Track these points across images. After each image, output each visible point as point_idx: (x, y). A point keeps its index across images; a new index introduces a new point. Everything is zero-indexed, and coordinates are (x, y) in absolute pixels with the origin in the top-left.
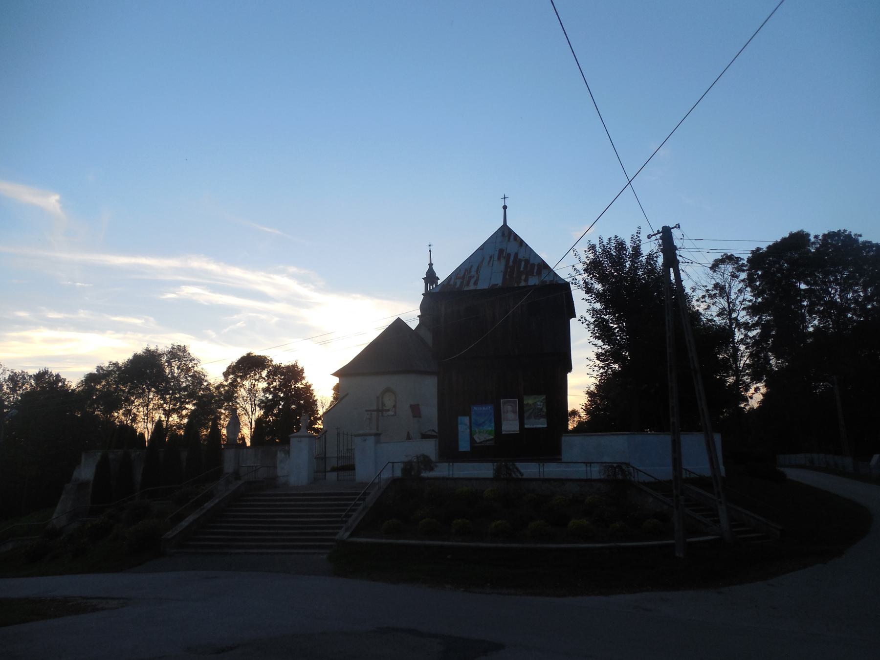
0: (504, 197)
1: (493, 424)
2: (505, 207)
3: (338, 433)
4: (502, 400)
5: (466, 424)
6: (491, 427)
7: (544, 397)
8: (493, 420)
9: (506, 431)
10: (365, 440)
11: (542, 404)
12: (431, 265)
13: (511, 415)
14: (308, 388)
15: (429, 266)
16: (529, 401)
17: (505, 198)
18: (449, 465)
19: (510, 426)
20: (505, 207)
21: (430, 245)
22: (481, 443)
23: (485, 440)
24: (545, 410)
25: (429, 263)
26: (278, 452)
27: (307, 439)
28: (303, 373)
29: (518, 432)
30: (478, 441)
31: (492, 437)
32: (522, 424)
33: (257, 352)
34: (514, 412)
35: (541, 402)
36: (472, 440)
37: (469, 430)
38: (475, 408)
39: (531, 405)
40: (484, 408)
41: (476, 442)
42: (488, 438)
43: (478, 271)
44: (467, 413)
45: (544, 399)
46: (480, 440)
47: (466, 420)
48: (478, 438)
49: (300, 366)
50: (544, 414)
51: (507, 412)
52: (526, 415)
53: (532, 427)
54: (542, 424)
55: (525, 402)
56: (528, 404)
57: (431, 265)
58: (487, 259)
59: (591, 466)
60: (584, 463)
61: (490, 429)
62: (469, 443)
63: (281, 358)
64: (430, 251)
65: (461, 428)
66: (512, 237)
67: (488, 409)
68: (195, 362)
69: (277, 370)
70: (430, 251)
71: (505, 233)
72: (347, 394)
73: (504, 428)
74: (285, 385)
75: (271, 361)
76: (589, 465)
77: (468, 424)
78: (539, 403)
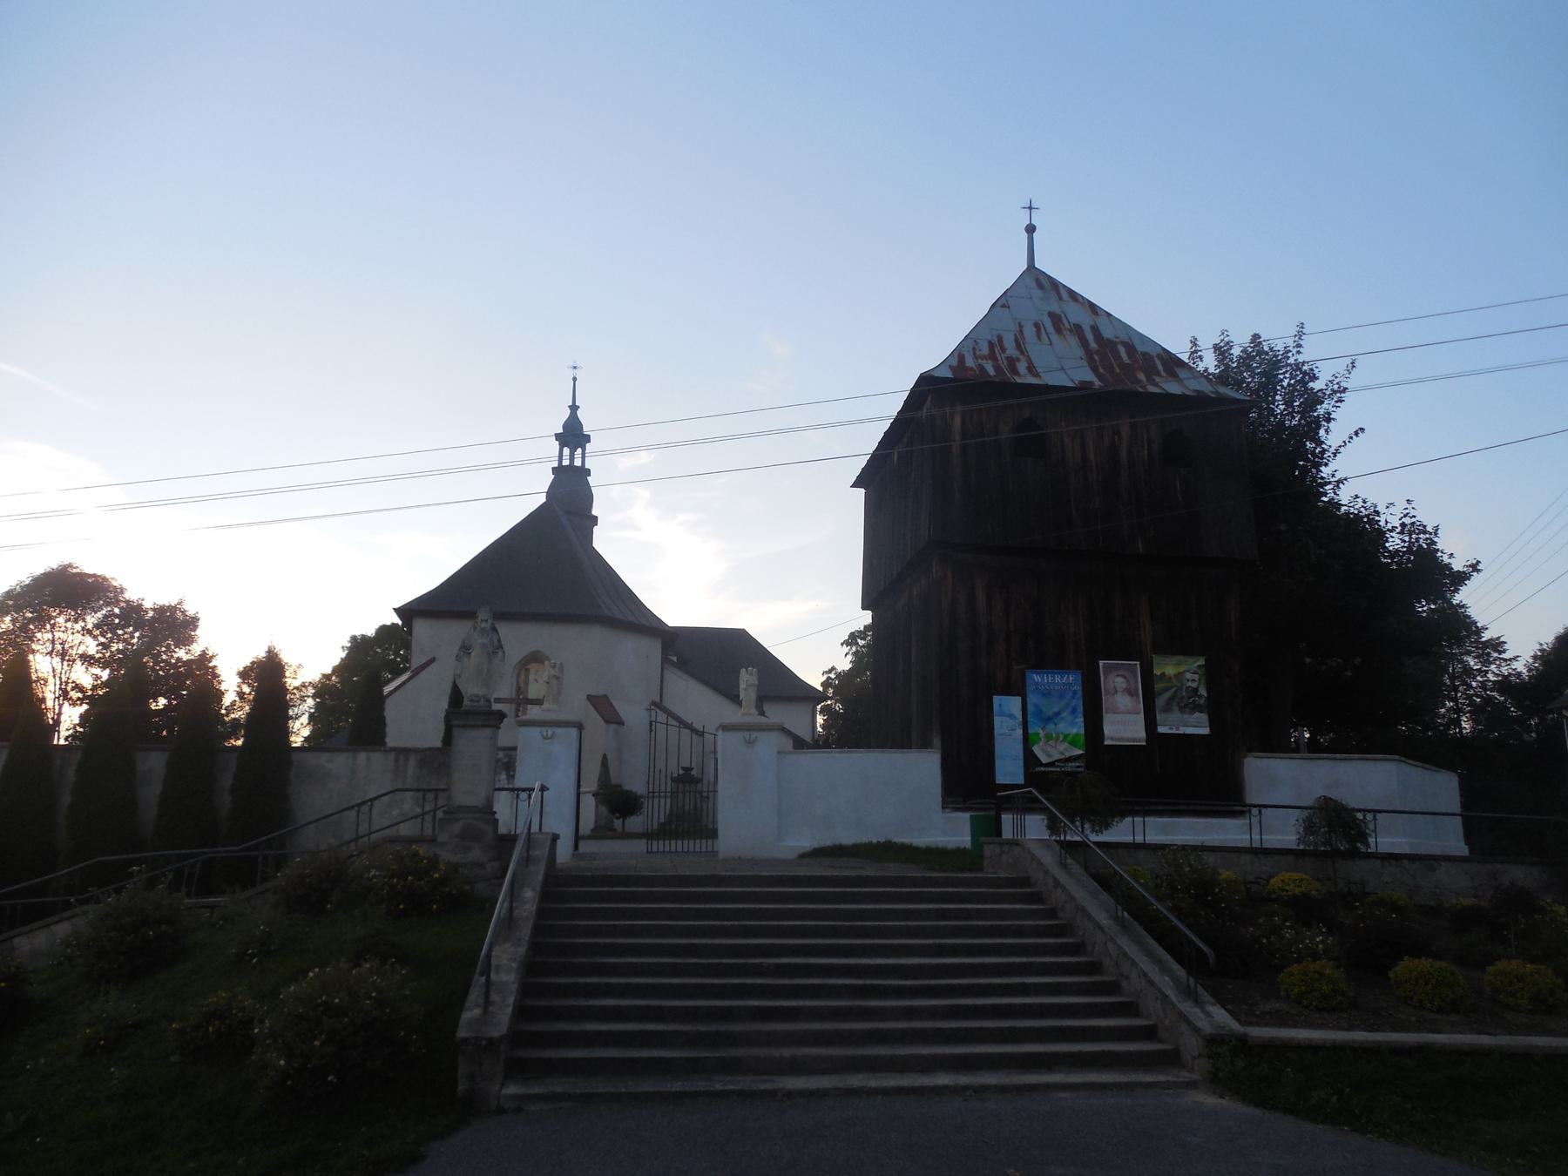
0: (1033, 211)
1: (1080, 719)
2: (1031, 229)
3: (651, 722)
4: (1101, 663)
5: (1012, 716)
6: (1077, 728)
7: (1201, 662)
8: (1081, 708)
9: (1112, 739)
10: (750, 743)
12: (574, 408)
13: (1123, 701)
14: (204, 658)
15: (569, 411)
16: (1166, 667)
20: (1031, 229)
22: (1052, 764)
24: (1203, 692)
25: (571, 404)
26: (1483, 639)
28: (195, 627)
29: (1144, 744)
30: (1045, 760)
31: (1081, 752)
33: (88, 564)
34: (1130, 692)
35: (1195, 673)
36: (1030, 758)
37: (1020, 732)
38: (1037, 678)
39: (1170, 678)
40: (1057, 679)
41: (1039, 762)
42: (1068, 755)
43: (1019, 346)
44: (1015, 687)
45: (1199, 666)
46: (1049, 756)
47: (1012, 704)
50: (1202, 702)
51: (1116, 692)
52: (1160, 702)
53: (1174, 731)
54: (1197, 725)
55: (1157, 672)
57: (574, 408)
58: (1029, 332)
61: (1074, 731)
62: (1021, 763)
64: (575, 379)
65: (1000, 725)
66: (1065, 295)
67: (1070, 680)
69: (133, 613)
70: (575, 379)
71: (1036, 280)
72: (432, 660)
74: (148, 647)
75: (122, 590)
77: (1019, 715)
78: (1188, 676)
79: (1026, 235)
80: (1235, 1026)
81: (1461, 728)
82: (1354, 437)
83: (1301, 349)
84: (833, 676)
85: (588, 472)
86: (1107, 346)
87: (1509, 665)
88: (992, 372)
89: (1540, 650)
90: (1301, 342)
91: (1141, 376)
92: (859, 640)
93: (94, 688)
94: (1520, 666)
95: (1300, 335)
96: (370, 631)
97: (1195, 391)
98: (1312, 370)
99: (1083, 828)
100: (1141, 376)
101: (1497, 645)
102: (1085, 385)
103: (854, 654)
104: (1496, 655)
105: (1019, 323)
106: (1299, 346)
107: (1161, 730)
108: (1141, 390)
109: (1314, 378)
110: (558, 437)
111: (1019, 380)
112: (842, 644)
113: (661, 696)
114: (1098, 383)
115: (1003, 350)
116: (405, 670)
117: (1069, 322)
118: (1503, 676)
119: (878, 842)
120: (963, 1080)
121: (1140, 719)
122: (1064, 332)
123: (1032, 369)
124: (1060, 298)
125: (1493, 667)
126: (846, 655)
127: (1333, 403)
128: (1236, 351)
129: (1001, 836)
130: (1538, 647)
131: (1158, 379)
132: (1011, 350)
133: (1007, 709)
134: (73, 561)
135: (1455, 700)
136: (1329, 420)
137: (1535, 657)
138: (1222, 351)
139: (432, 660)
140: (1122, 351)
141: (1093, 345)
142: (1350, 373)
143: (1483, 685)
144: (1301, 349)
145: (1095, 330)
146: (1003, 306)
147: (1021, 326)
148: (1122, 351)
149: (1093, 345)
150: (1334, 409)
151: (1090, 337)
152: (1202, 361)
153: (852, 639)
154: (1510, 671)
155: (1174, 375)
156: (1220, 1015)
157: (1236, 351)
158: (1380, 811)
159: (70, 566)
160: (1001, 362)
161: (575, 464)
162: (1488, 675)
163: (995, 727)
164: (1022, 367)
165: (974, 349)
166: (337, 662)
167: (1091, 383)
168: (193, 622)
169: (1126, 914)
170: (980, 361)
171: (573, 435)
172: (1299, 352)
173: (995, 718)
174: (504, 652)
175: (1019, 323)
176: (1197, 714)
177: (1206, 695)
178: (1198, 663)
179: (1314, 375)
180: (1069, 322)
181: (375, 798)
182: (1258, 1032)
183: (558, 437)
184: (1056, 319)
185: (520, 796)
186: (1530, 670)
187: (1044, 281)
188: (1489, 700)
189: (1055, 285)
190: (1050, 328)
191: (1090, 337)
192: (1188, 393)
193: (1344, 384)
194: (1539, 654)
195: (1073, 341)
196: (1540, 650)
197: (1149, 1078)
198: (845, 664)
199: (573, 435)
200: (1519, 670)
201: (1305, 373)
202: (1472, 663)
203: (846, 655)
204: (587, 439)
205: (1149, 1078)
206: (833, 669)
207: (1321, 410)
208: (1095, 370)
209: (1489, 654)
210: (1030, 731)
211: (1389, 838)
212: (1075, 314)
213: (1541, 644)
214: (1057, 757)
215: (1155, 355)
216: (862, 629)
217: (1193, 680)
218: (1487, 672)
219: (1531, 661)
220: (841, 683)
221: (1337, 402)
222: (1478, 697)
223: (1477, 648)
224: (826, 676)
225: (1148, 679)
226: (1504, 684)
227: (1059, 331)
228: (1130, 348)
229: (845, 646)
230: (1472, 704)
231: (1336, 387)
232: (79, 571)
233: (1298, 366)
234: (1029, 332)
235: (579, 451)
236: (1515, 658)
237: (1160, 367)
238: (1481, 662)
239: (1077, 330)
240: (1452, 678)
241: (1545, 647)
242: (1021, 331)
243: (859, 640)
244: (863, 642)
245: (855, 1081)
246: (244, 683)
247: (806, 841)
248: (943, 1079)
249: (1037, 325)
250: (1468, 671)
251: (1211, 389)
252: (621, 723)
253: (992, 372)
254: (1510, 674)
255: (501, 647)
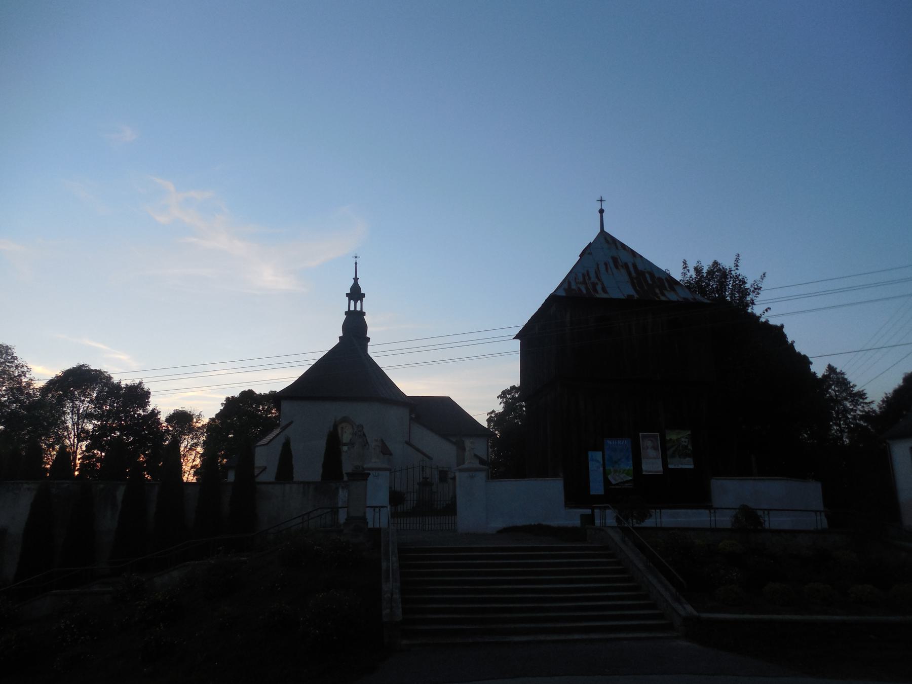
2: (601, 211)
4: (640, 434)
5: (598, 461)
6: (629, 466)
7: (689, 432)
9: (646, 471)
11: (687, 440)
12: (356, 279)
13: (651, 453)
16: (672, 436)
17: (601, 201)
18: (710, 512)
19: (652, 465)
21: (356, 257)
22: (617, 484)
23: (622, 481)
24: (690, 447)
26: (340, 490)
27: (388, 473)
29: (662, 473)
30: (614, 482)
31: (630, 478)
32: (665, 464)
34: (655, 448)
35: (687, 438)
36: (607, 482)
40: (619, 442)
41: (610, 483)
42: (625, 480)
43: (597, 277)
44: (599, 447)
47: (598, 455)
48: (614, 479)
49: (146, 387)
51: (648, 448)
53: (676, 467)
54: (687, 464)
55: (668, 438)
56: (671, 439)
57: (356, 279)
58: (602, 268)
59: (769, 513)
60: (812, 511)
61: (628, 468)
63: (123, 376)
64: (356, 263)
65: (592, 466)
66: (619, 246)
68: (25, 369)
70: (356, 263)
71: (605, 239)
73: (644, 467)
76: (818, 513)
77: (601, 460)
79: (599, 214)
80: (695, 613)
81: (843, 442)
82: (766, 312)
83: (738, 268)
84: (493, 415)
85: (364, 314)
86: (640, 274)
87: (869, 406)
88: (585, 292)
89: (885, 397)
90: (738, 264)
91: (657, 291)
92: (508, 395)
93: (94, 430)
94: (875, 407)
95: (737, 260)
96: (237, 395)
97: (684, 298)
98: (743, 279)
99: (632, 521)
100: (657, 291)
101: (861, 395)
102: (630, 298)
103: (504, 403)
104: (861, 400)
105: (597, 263)
106: (737, 266)
107: (670, 466)
108: (657, 299)
109: (744, 283)
110: (347, 295)
111: (598, 296)
112: (498, 397)
113: (410, 438)
114: (636, 296)
115: (590, 278)
116: (278, 425)
117: (621, 262)
118: (865, 411)
119: (535, 524)
120: (584, 637)
121: (660, 462)
122: (619, 268)
123: (604, 290)
124: (617, 248)
125: (860, 407)
126: (500, 404)
127: (754, 294)
128: (705, 271)
129: (594, 525)
130: (885, 395)
131: (666, 293)
132: (594, 279)
133: (595, 457)
134: (85, 363)
135: (839, 425)
136: (753, 303)
137: (883, 401)
138: (698, 270)
139: (291, 423)
140: (647, 276)
141: (634, 274)
142: (763, 280)
143: (854, 418)
144: (738, 268)
145: (635, 266)
146: (589, 254)
147: (598, 265)
148: (647, 276)
149: (634, 274)
150: (755, 298)
151: (632, 269)
152: (689, 272)
153: (503, 395)
154: (869, 409)
155: (674, 290)
156: (689, 608)
157: (705, 271)
158: (771, 510)
159: (83, 365)
160: (588, 285)
161: (357, 310)
162: (857, 412)
163: (590, 467)
164: (599, 288)
165: (575, 279)
166: (218, 411)
167: (633, 296)
168: (147, 394)
169: (651, 564)
170: (579, 285)
171: (356, 294)
172: (737, 269)
173: (590, 463)
174: (369, 445)
175: (597, 263)
176: (687, 459)
177: (691, 449)
178: (688, 433)
179: (745, 281)
180: (621, 262)
181: (311, 512)
182: (705, 615)
183: (347, 295)
184: (615, 260)
185: (376, 510)
186: (880, 408)
187: (609, 239)
188: (857, 425)
189: (614, 241)
190: (612, 265)
191: (632, 269)
192: (680, 300)
193: (759, 285)
194: (885, 399)
195: (623, 271)
196: (885, 397)
197: (661, 635)
198: (499, 408)
199: (356, 294)
200: (874, 409)
201: (740, 281)
202: (848, 405)
203: (500, 404)
204: (364, 295)
205: (661, 635)
206: (493, 411)
207: (748, 299)
208: (637, 291)
209: (857, 400)
210: (607, 468)
211: (775, 522)
212: (624, 257)
213: (886, 394)
214: (620, 481)
215: (664, 278)
216: (509, 389)
217: (685, 442)
218: (856, 410)
219: (881, 403)
220: (496, 419)
221: (756, 294)
222: (852, 424)
223: (851, 397)
224: (489, 416)
225: (663, 441)
226: (867, 416)
227: (617, 267)
228: (652, 275)
229: (499, 398)
230: (849, 427)
231: (756, 287)
232: (87, 368)
233: (737, 277)
234: (602, 268)
235: (359, 302)
236: (872, 402)
237: (666, 284)
238: (853, 404)
239: (626, 266)
240: (837, 413)
241: (888, 395)
242: (598, 268)
243: (508, 395)
244: (510, 396)
245: (542, 637)
246: (169, 425)
247: (498, 524)
248: (576, 637)
249: (606, 264)
250: (846, 411)
251: (693, 297)
252: (391, 454)
253: (585, 292)
254: (869, 411)
255: (367, 443)
